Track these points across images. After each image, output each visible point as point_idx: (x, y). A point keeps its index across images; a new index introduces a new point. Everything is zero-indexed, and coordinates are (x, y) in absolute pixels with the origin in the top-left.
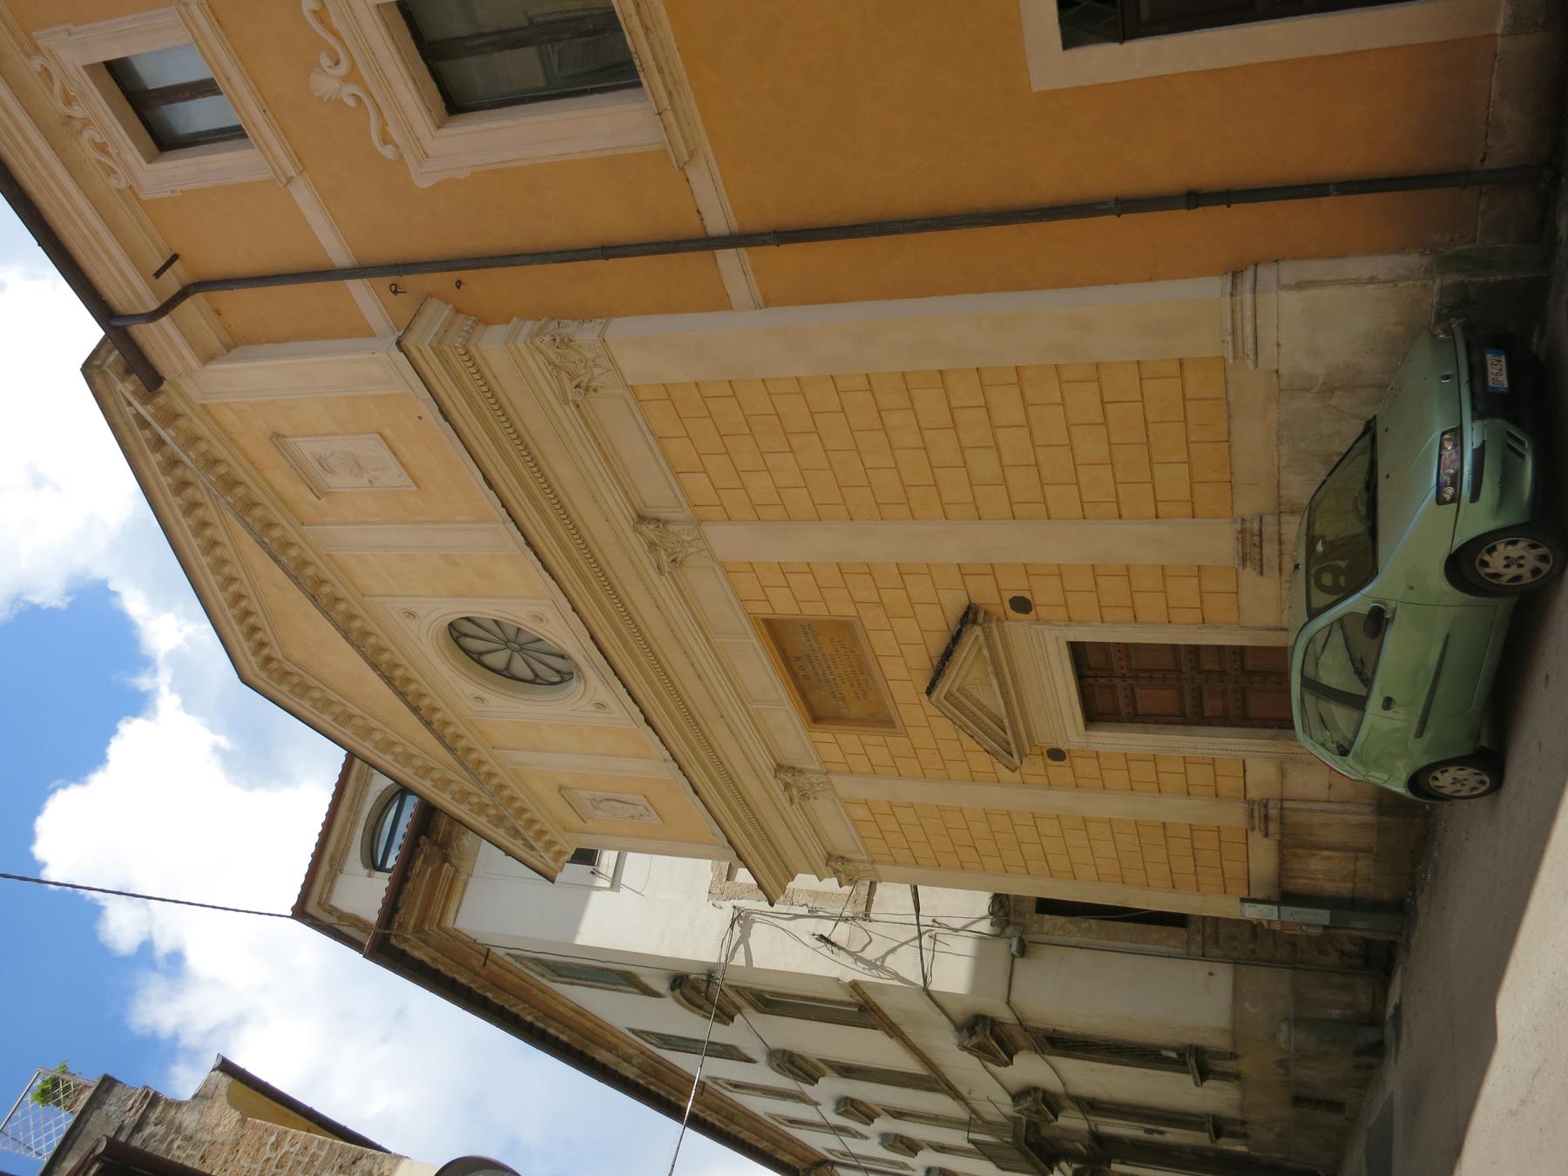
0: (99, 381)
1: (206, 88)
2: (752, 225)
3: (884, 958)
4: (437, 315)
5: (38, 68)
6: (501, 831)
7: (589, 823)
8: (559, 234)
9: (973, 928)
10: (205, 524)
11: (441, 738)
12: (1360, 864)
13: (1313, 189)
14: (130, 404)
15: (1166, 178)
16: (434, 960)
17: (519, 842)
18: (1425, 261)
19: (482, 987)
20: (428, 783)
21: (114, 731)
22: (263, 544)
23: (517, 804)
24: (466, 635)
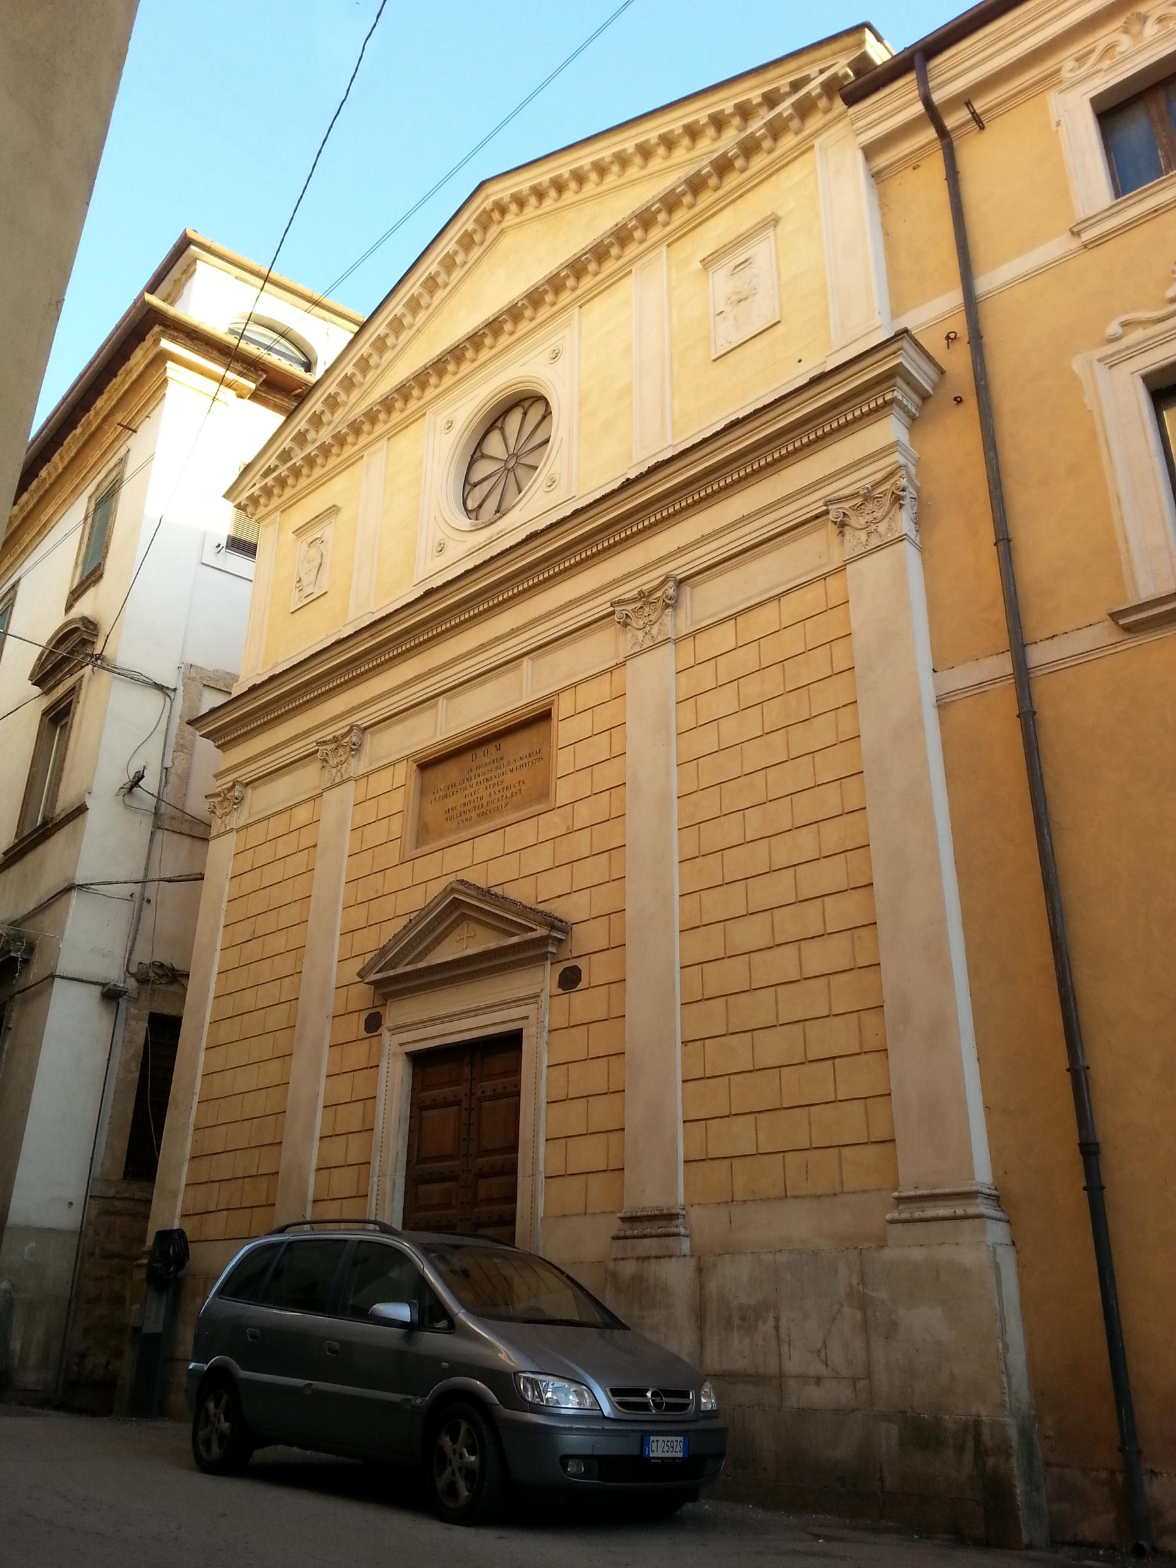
14: (821, 72)
15: (1110, 1121)
16: (129, 373)
24: (525, 414)
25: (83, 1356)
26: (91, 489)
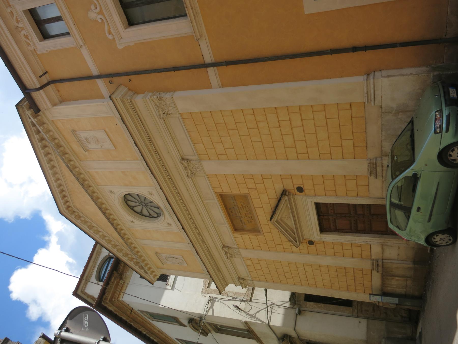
0: (21, 110)
1: (59, 19)
2: (219, 60)
3: (256, 314)
4: (123, 90)
5: (10, 11)
6: (137, 267)
7: (165, 265)
8: (160, 64)
9: (284, 305)
10: (51, 160)
11: (119, 234)
12: (408, 282)
13: (392, 45)
14: (30, 118)
15: (346, 43)
16: (115, 311)
17: (143, 271)
18: (428, 69)
19: (130, 321)
20: (115, 250)
21: (36, 252)
22: (68, 166)
23: (143, 258)
24: (129, 200)
25: (402, 317)
26: (149, 320)
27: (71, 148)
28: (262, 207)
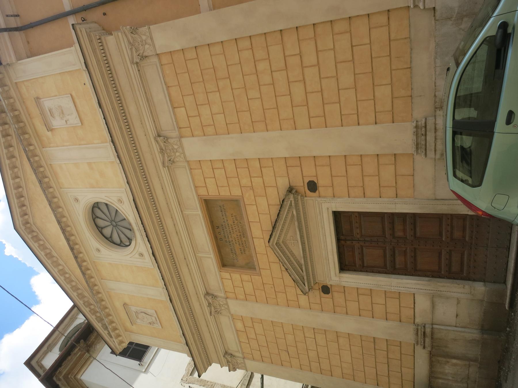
11: (80, 266)
12: (471, 370)
17: (106, 332)
22: (25, 150)
27: (35, 128)
28: (258, 217)
